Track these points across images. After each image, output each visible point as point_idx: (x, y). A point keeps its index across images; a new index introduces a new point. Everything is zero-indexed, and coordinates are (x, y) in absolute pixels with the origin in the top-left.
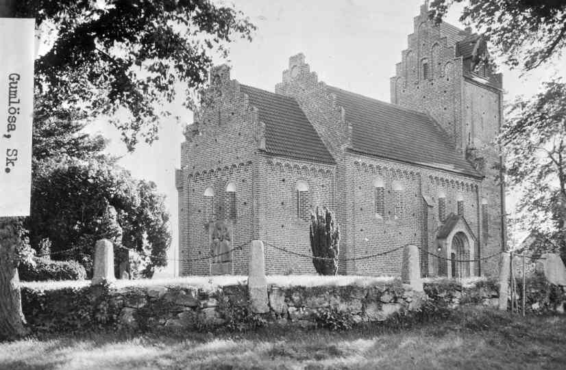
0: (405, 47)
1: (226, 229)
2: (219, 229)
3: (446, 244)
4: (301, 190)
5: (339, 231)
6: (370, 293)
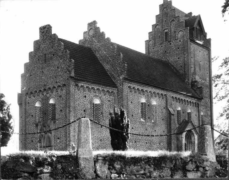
0: (154, 22)
1: (49, 126)
2: (45, 127)
3: (182, 137)
4: (96, 103)
5: (129, 123)
6: (178, 163)
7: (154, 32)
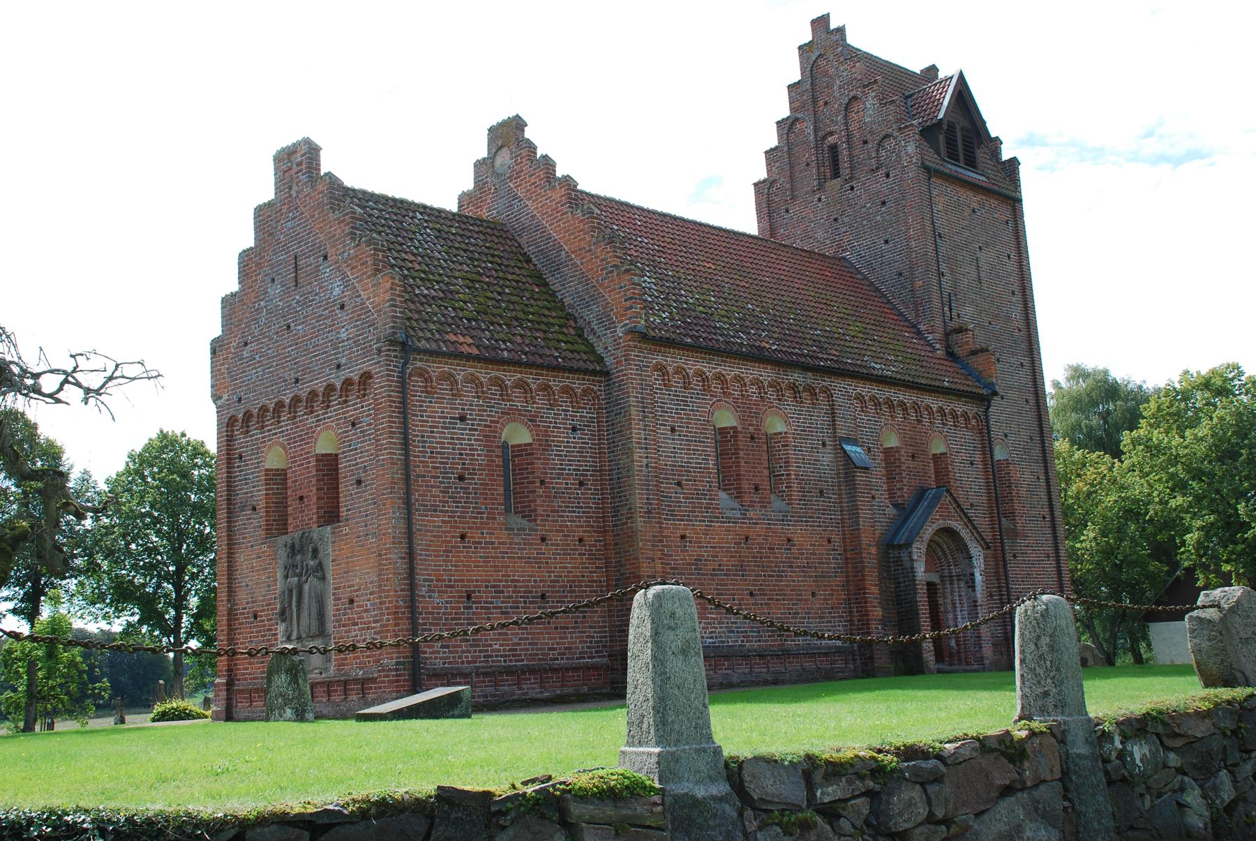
7: (786, 149)
